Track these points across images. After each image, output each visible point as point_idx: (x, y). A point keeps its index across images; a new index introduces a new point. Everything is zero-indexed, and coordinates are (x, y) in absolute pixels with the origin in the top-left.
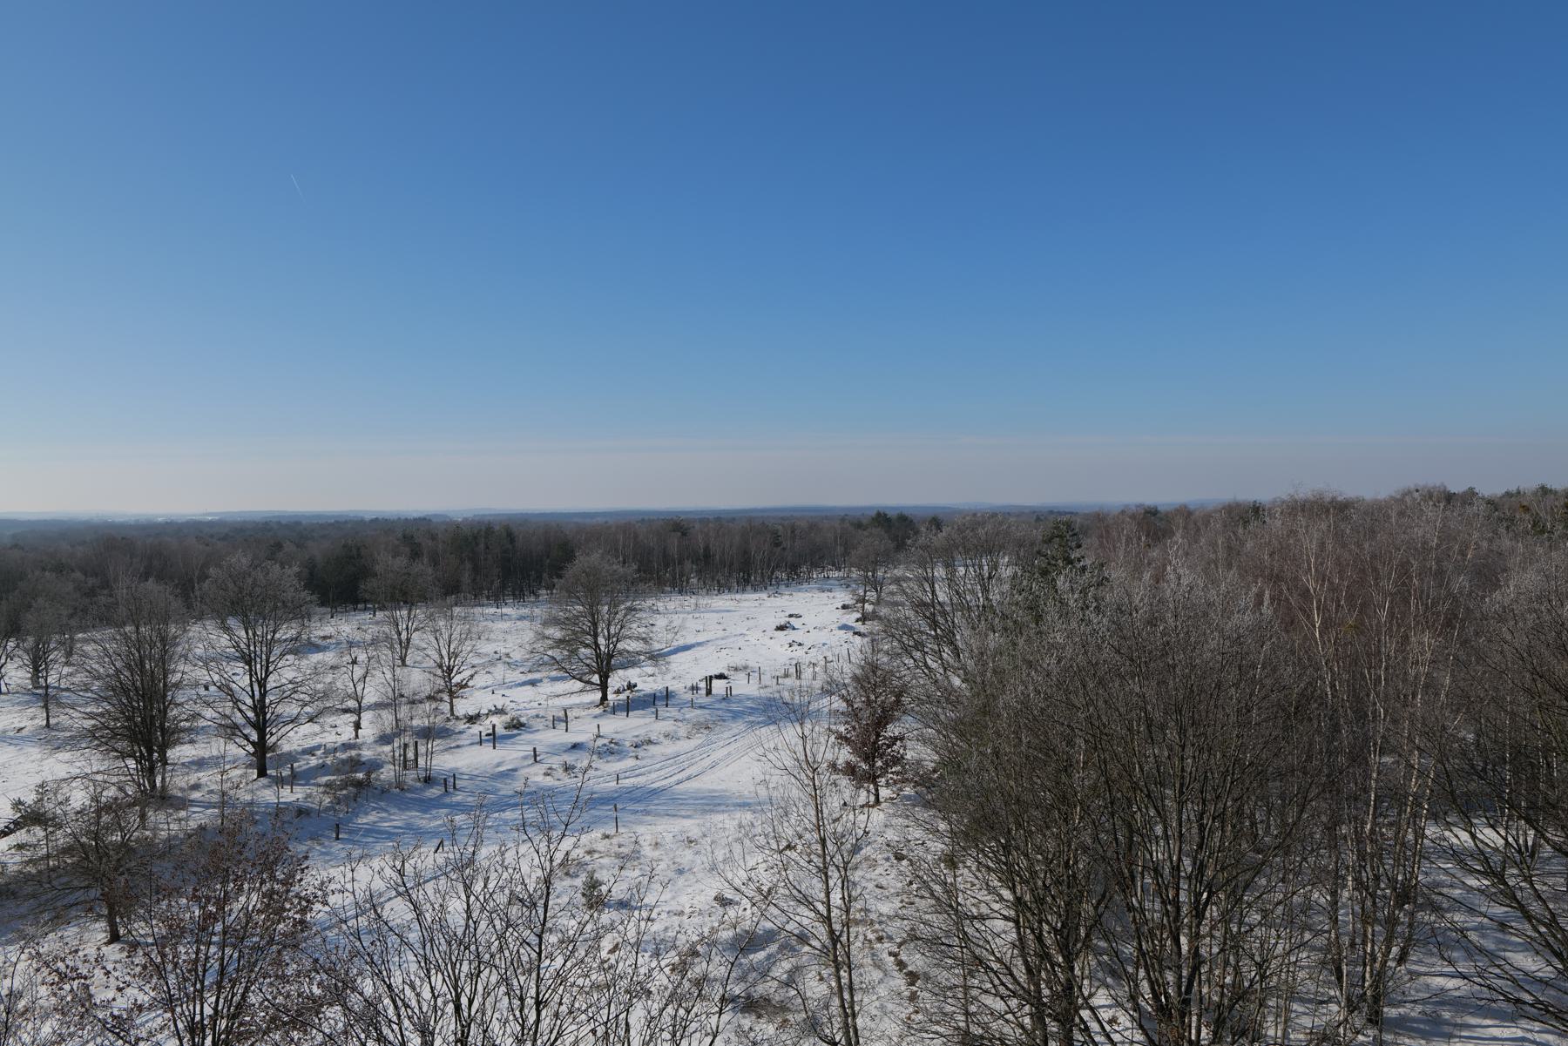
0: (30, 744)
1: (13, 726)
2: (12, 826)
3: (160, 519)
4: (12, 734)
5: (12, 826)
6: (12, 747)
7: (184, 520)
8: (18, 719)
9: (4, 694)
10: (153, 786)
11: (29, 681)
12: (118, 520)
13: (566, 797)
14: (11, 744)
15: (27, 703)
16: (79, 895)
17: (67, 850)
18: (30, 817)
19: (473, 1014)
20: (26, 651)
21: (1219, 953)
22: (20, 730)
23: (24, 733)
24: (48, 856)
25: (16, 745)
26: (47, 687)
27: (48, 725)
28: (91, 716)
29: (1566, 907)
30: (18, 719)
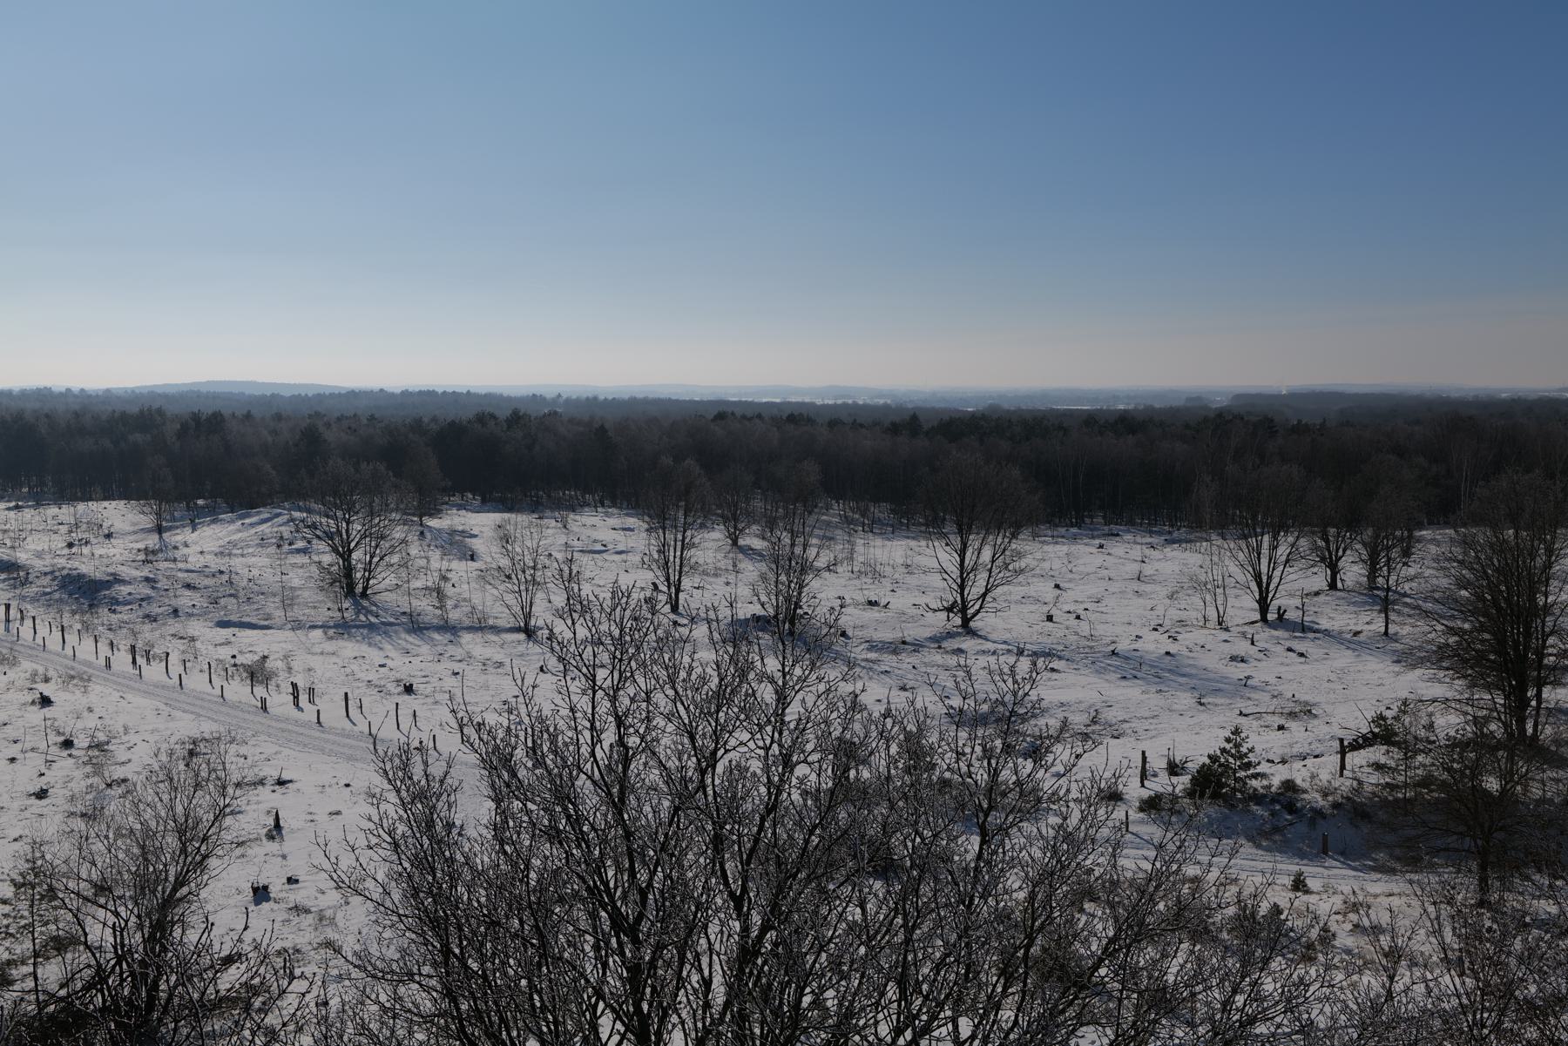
0: (1368, 651)
1: (1349, 628)
2: (1361, 741)
3: (1504, 395)
4: (1349, 636)
5: (1361, 741)
6: (1350, 652)
7: (1533, 396)
8: (1354, 621)
9: (1340, 590)
10: (1523, 730)
11: (1366, 579)
12: (1454, 395)
13: (1082, 707)
14: (1348, 648)
15: (1365, 603)
16: (1451, 840)
17: (1426, 782)
18: (1382, 734)
19: (210, 833)
20: (1364, 544)
21: (806, 954)
22: (1357, 633)
23: (1362, 638)
24: (1406, 785)
25: (1354, 650)
26: (1388, 589)
27: (1386, 633)
28: (1451, 631)
29: (1494, 1045)
30: (1354, 621)
